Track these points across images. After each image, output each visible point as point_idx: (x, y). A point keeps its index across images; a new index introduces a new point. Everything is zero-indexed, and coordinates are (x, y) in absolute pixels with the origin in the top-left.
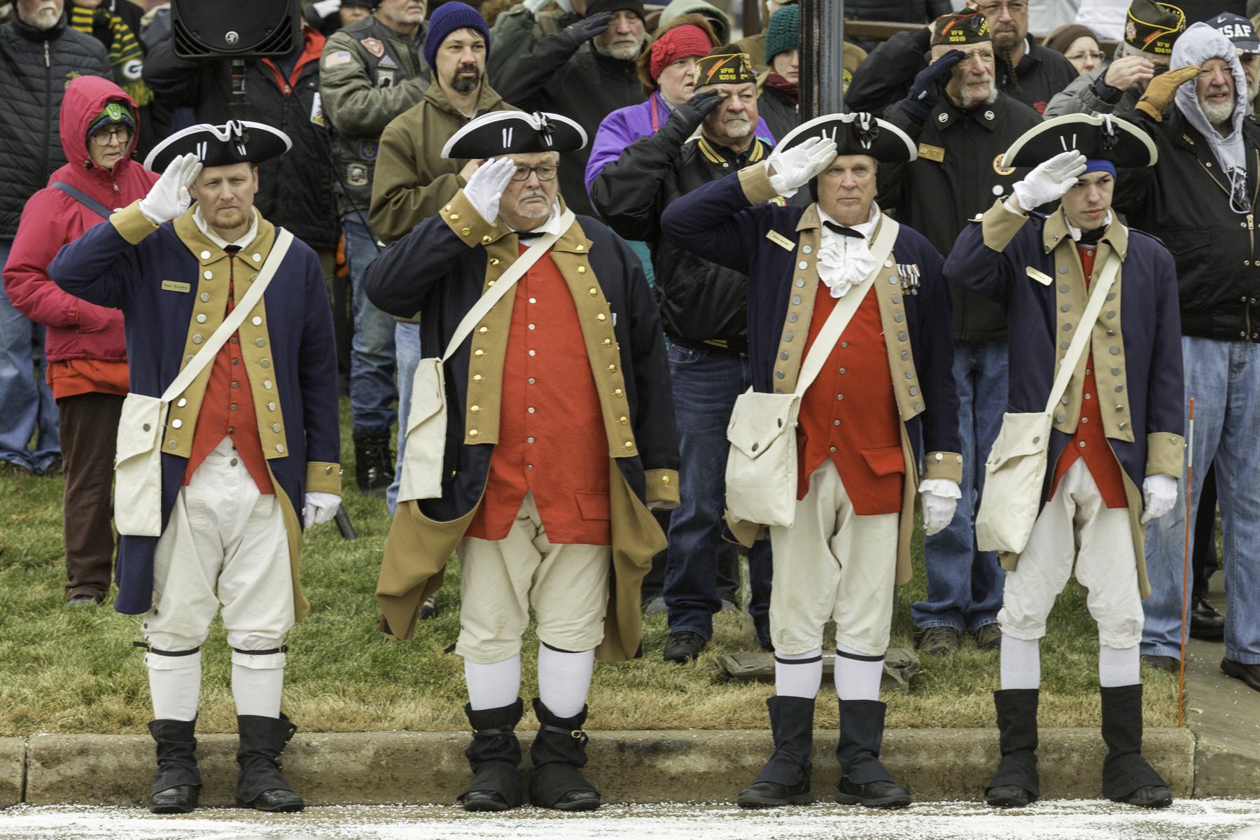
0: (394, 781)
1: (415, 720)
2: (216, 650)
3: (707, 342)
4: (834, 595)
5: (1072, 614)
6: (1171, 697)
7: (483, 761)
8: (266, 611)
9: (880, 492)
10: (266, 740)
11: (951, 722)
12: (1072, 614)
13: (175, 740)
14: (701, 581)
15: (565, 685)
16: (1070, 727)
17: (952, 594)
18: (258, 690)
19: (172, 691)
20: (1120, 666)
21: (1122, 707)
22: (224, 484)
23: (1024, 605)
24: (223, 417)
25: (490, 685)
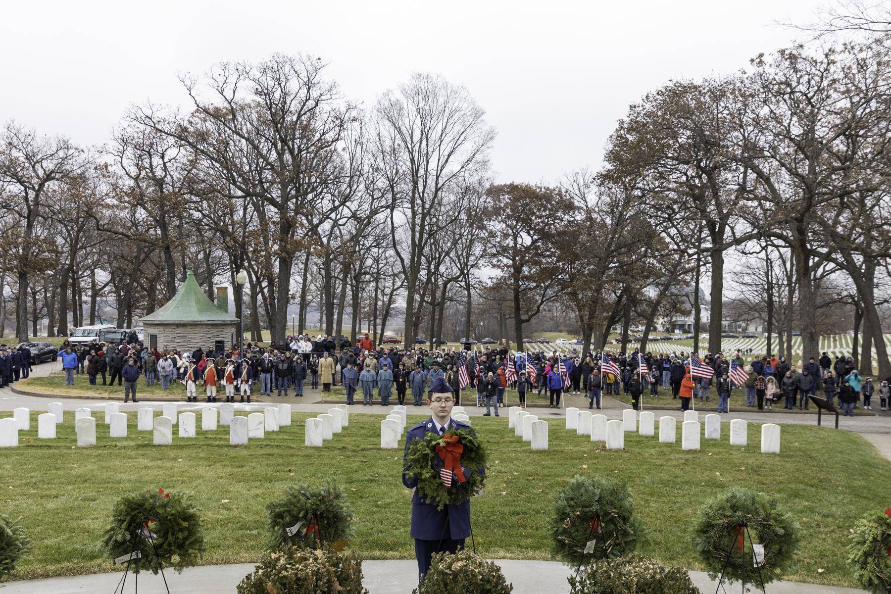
0: (203, 400)
1: (203, 396)
2: (191, 392)
3: (582, 376)
4: (230, 390)
5: (245, 391)
6: (676, 477)
7: (250, 413)
8: (194, 390)
9: (231, 383)
10: (195, 398)
11: (238, 398)
12: (245, 391)
13: (189, 398)
14: (221, 389)
15: (214, 395)
16: (245, 397)
17: (237, 389)
18: (194, 395)
19: (189, 395)
20: (248, 394)
21: (248, 397)
22: (190, 382)
23: (242, 390)
24: (190, 378)
25: (209, 395)
